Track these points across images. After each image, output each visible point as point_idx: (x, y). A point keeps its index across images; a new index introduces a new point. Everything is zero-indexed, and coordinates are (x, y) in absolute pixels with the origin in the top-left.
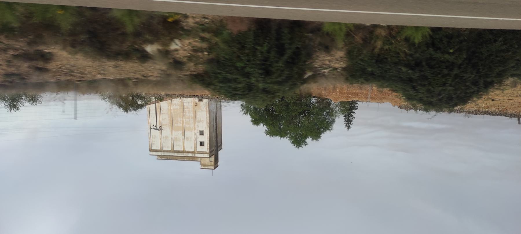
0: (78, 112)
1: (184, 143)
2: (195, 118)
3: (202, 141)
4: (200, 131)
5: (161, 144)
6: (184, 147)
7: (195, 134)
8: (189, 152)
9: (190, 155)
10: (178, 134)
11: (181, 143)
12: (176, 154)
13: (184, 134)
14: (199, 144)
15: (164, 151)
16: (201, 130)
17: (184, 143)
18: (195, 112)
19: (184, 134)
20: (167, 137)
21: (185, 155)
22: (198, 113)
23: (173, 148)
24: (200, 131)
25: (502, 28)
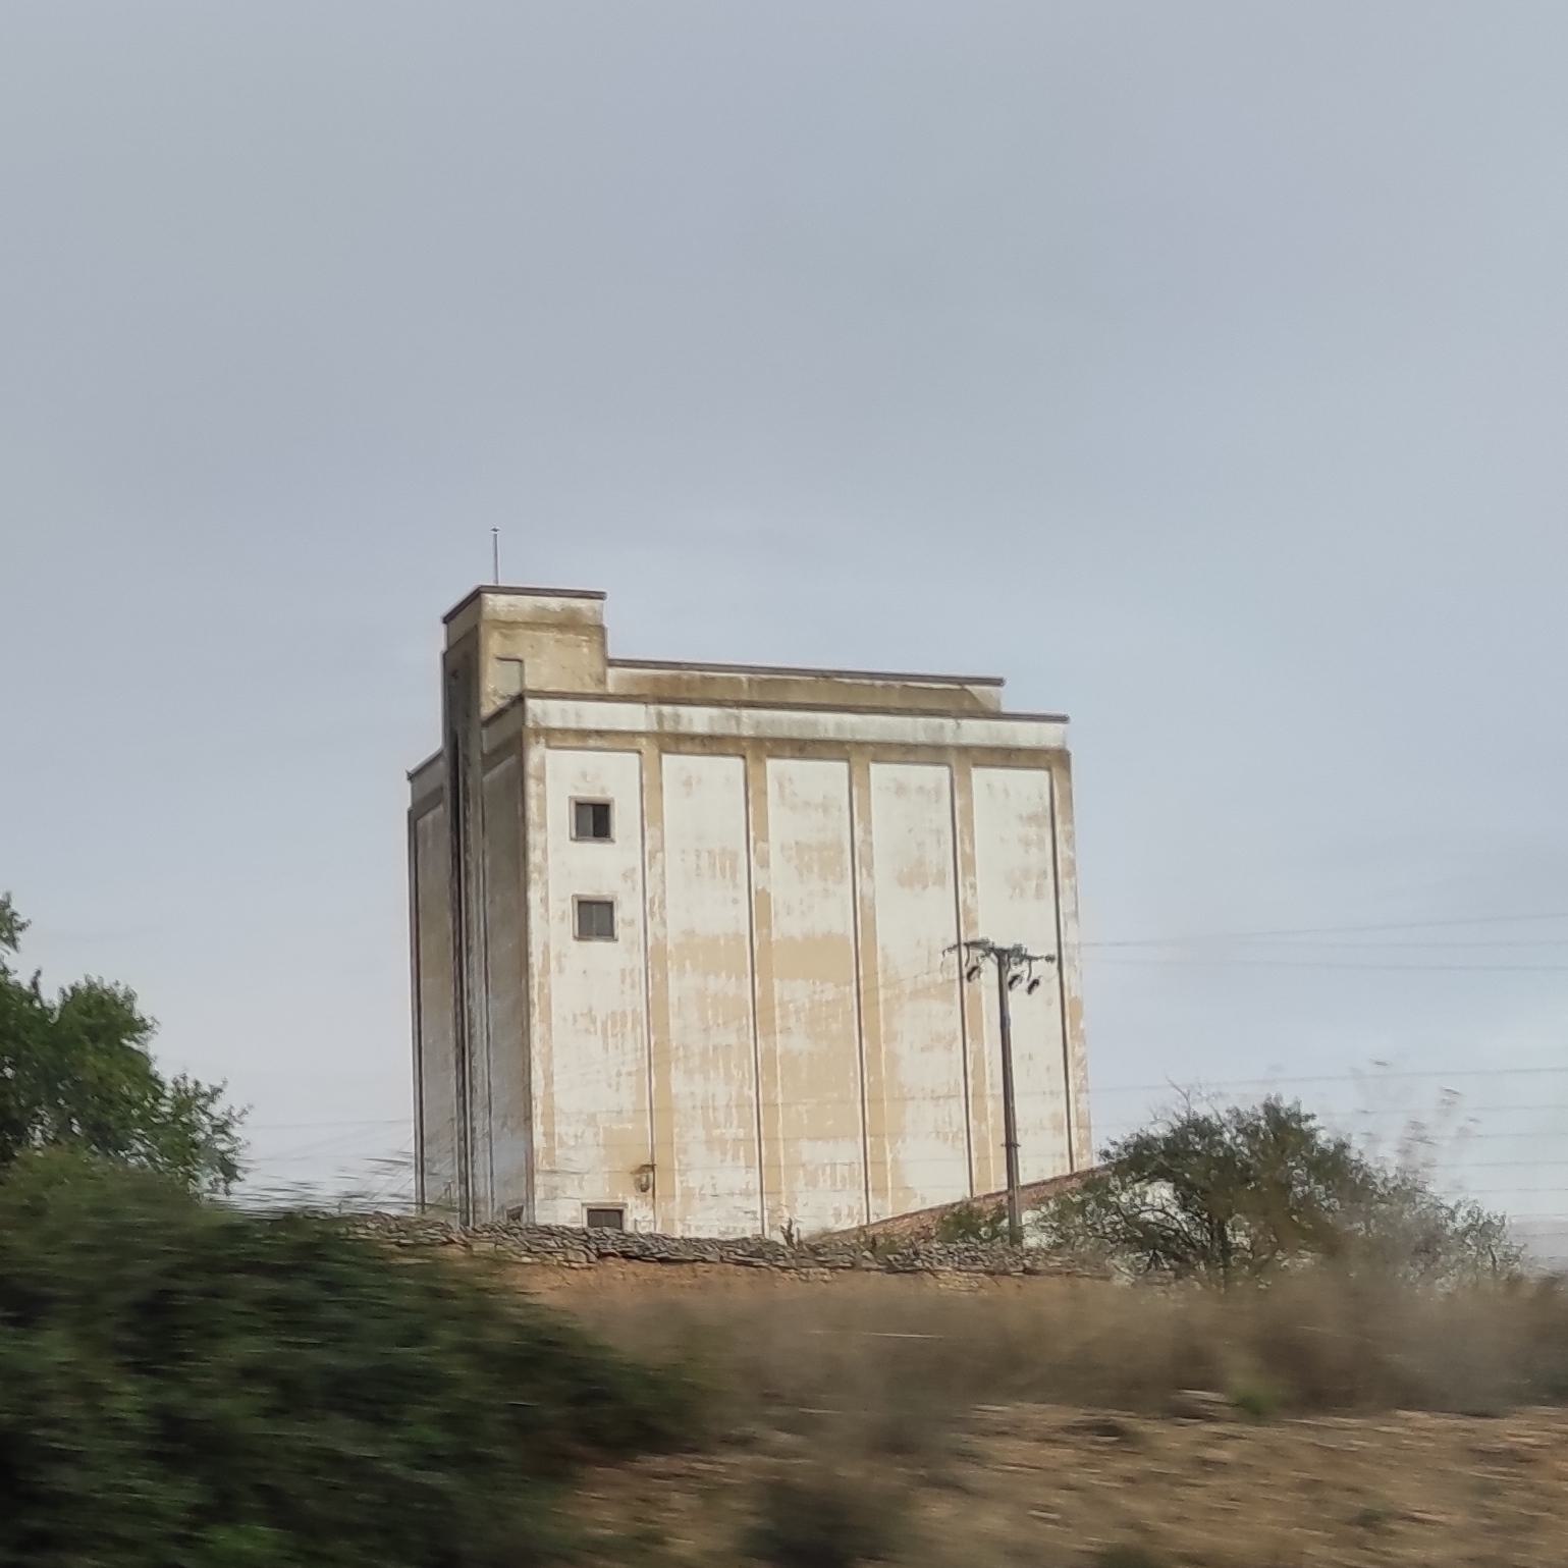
1: (755, 826)
2: (658, 1058)
3: (593, 849)
5: (959, 822)
6: (753, 792)
7: (652, 907)
8: (711, 744)
9: (699, 719)
10: (811, 910)
11: (781, 824)
12: (829, 724)
13: (759, 906)
14: (619, 821)
15: (933, 753)
16: (598, 946)
17: (755, 826)
18: (659, 1108)
19: (759, 906)
20: (913, 877)
21: (750, 721)
23: (857, 783)
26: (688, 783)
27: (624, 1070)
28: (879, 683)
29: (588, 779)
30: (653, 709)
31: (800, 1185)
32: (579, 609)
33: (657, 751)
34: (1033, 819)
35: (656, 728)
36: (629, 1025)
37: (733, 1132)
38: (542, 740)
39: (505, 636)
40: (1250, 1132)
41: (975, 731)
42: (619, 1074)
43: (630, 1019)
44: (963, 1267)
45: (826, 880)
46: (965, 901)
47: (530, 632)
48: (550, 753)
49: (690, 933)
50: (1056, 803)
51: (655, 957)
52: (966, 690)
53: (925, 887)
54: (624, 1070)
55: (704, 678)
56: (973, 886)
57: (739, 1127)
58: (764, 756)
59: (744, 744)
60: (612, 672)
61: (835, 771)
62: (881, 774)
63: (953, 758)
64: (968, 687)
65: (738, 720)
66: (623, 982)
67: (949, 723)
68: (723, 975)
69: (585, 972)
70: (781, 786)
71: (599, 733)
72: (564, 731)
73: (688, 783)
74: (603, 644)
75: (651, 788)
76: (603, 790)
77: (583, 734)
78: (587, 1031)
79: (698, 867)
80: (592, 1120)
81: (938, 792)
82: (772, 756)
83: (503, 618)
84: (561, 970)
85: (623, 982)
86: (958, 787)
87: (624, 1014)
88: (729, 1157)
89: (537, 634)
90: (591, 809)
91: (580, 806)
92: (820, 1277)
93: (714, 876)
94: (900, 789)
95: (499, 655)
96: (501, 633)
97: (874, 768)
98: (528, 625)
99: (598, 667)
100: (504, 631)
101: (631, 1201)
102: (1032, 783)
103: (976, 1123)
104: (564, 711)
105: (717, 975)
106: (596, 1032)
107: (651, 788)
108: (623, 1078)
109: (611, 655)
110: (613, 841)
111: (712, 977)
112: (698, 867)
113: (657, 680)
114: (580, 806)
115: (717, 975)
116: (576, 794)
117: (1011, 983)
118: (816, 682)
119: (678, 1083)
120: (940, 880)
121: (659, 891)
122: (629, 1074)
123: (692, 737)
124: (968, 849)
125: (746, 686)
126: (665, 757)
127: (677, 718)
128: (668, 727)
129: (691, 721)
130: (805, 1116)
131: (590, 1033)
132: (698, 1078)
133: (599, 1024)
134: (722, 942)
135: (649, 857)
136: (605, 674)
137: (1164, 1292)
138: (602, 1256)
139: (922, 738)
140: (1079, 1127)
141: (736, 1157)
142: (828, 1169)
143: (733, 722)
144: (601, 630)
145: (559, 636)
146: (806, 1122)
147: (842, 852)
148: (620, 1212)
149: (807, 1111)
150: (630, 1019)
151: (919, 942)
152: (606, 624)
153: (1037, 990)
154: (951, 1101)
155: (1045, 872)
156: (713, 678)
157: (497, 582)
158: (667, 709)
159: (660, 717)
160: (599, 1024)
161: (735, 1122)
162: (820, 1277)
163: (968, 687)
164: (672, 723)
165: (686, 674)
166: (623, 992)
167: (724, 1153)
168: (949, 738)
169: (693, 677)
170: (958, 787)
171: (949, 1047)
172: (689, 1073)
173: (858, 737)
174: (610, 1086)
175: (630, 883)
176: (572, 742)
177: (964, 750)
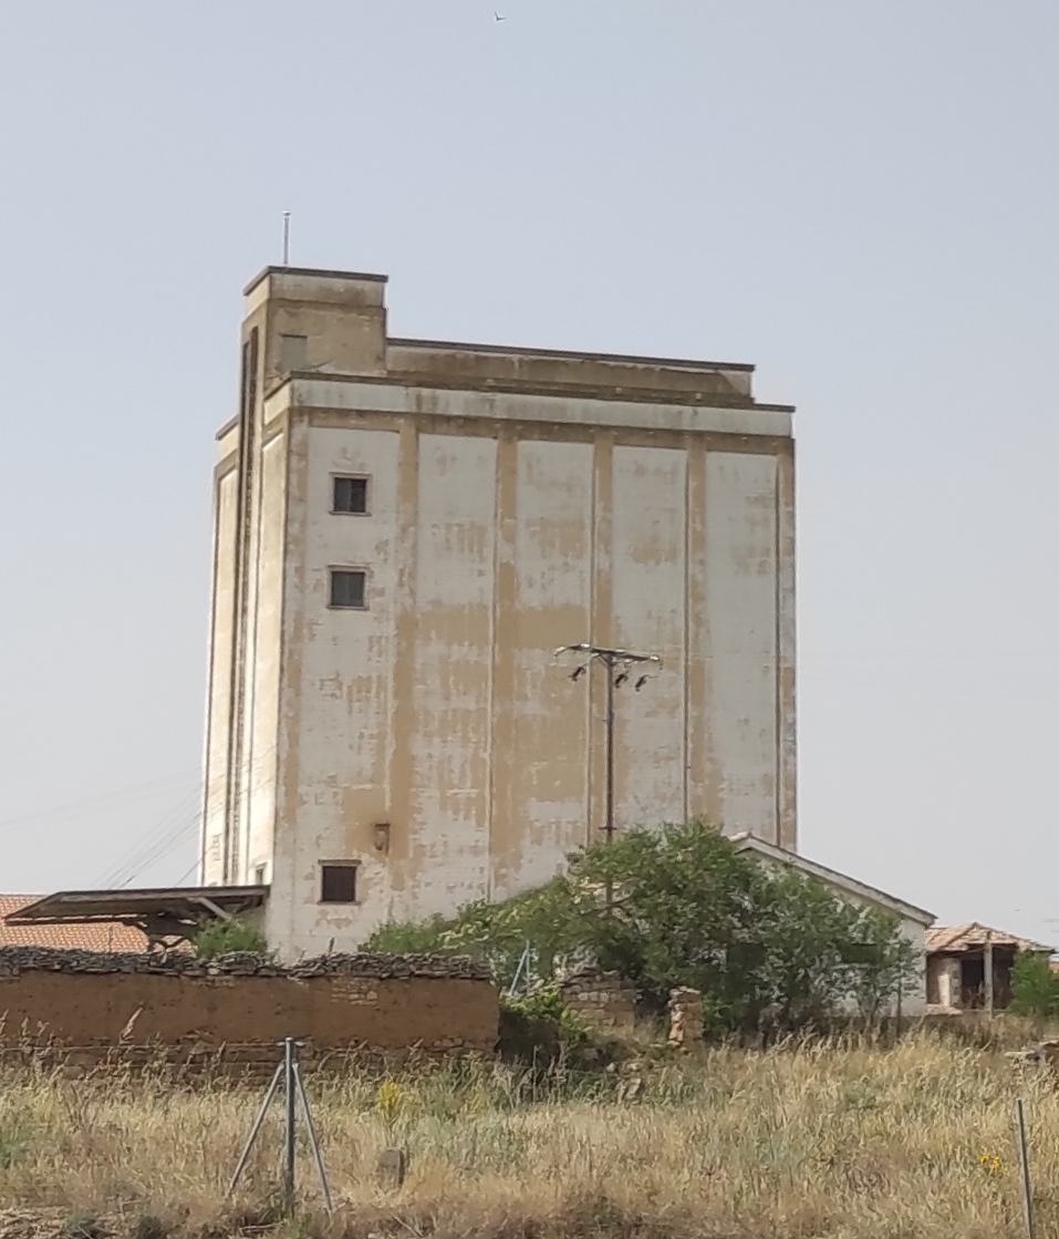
0: (774, 617)
1: (507, 503)
2: (405, 721)
3: (348, 521)
4: (338, 576)
5: (696, 501)
6: (506, 471)
7: (408, 577)
8: (469, 425)
9: (456, 401)
10: (554, 584)
11: (530, 502)
12: (577, 409)
13: (507, 579)
14: (376, 497)
15: (672, 437)
16: (348, 614)
17: (507, 503)
18: (404, 765)
19: (507, 579)
20: (647, 553)
21: (503, 404)
22: (366, 760)
23: (603, 463)
24: (338, 576)
25: (332, 492)
26: (442, 461)
27: (367, 732)
28: (640, 366)
29: (348, 456)
30: (413, 390)
31: (526, 842)
32: (363, 291)
33: (413, 431)
34: (760, 500)
35: (414, 409)
36: (374, 690)
37: (468, 791)
38: (306, 418)
39: (292, 315)
40: (678, 843)
41: (712, 418)
42: (362, 736)
43: (374, 686)
44: (355, 973)
45: (566, 555)
46: (693, 576)
47: (314, 311)
48: (314, 430)
49: (437, 603)
50: (781, 486)
51: (408, 626)
52: (722, 376)
53: (658, 563)
54: (367, 732)
55: (477, 358)
56: (702, 562)
57: (472, 787)
58: (515, 438)
59: (498, 426)
60: (391, 349)
61: (586, 450)
62: (624, 455)
63: (688, 440)
64: (722, 372)
65: (492, 402)
66: (370, 650)
67: (687, 410)
68: (466, 643)
69: (335, 639)
70: (530, 466)
71: (361, 413)
72: (327, 410)
73: (442, 461)
74: (384, 324)
75: (410, 465)
76: (362, 465)
77: (344, 413)
78: (333, 695)
79: (448, 540)
80: (333, 780)
81: (674, 472)
82: (522, 437)
83: (288, 297)
84: (312, 637)
85: (370, 650)
86: (696, 469)
87: (369, 678)
88: (461, 817)
89: (322, 313)
90: (350, 484)
91: (339, 482)
92: (225, 984)
93: (462, 550)
94: (640, 471)
95: (283, 331)
96: (288, 312)
97: (617, 449)
98: (310, 303)
99: (378, 345)
100: (289, 309)
101: (365, 858)
102: (761, 466)
103: (692, 783)
104: (327, 392)
105: (461, 644)
106: (341, 696)
107: (410, 465)
108: (366, 740)
109: (392, 333)
110: (369, 515)
111: (455, 647)
112: (448, 540)
113: (433, 357)
114: (339, 482)
115: (461, 644)
116: (336, 470)
117: (618, 681)
118: (582, 363)
119: (419, 748)
120: (672, 556)
121: (410, 561)
122: (372, 736)
123: (449, 419)
124: (698, 527)
125: (517, 365)
126: (423, 437)
127: (435, 400)
128: (425, 409)
129: (448, 404)
130: (534, 778)
131: (337, 698)
132: (437, 740)
133: (345, 689)
134: (466, 611)
135: (410, 525)
136: (384, 352)
137: (588, 982)
138: (24, 970)
139: (662, 424)
140: (787, 788)
141: (466, 817)
142: (554, 827)
143: (488, 406)
144: (382, 312)
145: (342, 315)
146: (535, 783)
147: (583, 528)
148: (353, 870)
149: (537, 771)
150: (374, 686)
151: (650, 613)
152: (387, 305)
153: (642, 687)
154: (671, 763)
155: (768, 550)
156: (486, 358)
157: (286, 262)
158: (426, 392)
159: (419, 399)
160: (345, 689)
161: (469, 784)
162: (225, 984)
163: (722, 372)
164: (430, 407)
165: (461, 354)
166: (370, 659)
167: (456, 812)
168: (685, 425)
169: (467, 356)
170: (696, 469)
171: (672, 712)
172: (429, 735)
173: (603, 422)
174: (351, 747)
175: (382, 556)
176: (334, 420)
177: (699, 435)
